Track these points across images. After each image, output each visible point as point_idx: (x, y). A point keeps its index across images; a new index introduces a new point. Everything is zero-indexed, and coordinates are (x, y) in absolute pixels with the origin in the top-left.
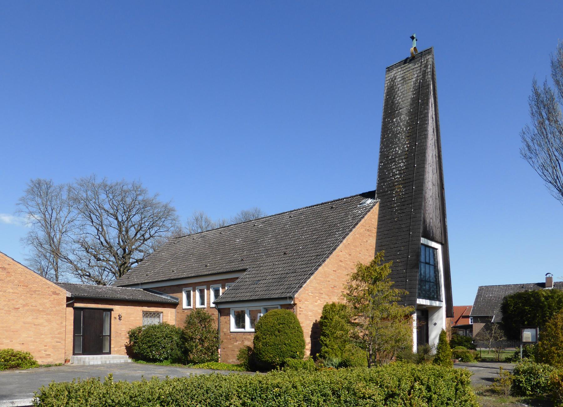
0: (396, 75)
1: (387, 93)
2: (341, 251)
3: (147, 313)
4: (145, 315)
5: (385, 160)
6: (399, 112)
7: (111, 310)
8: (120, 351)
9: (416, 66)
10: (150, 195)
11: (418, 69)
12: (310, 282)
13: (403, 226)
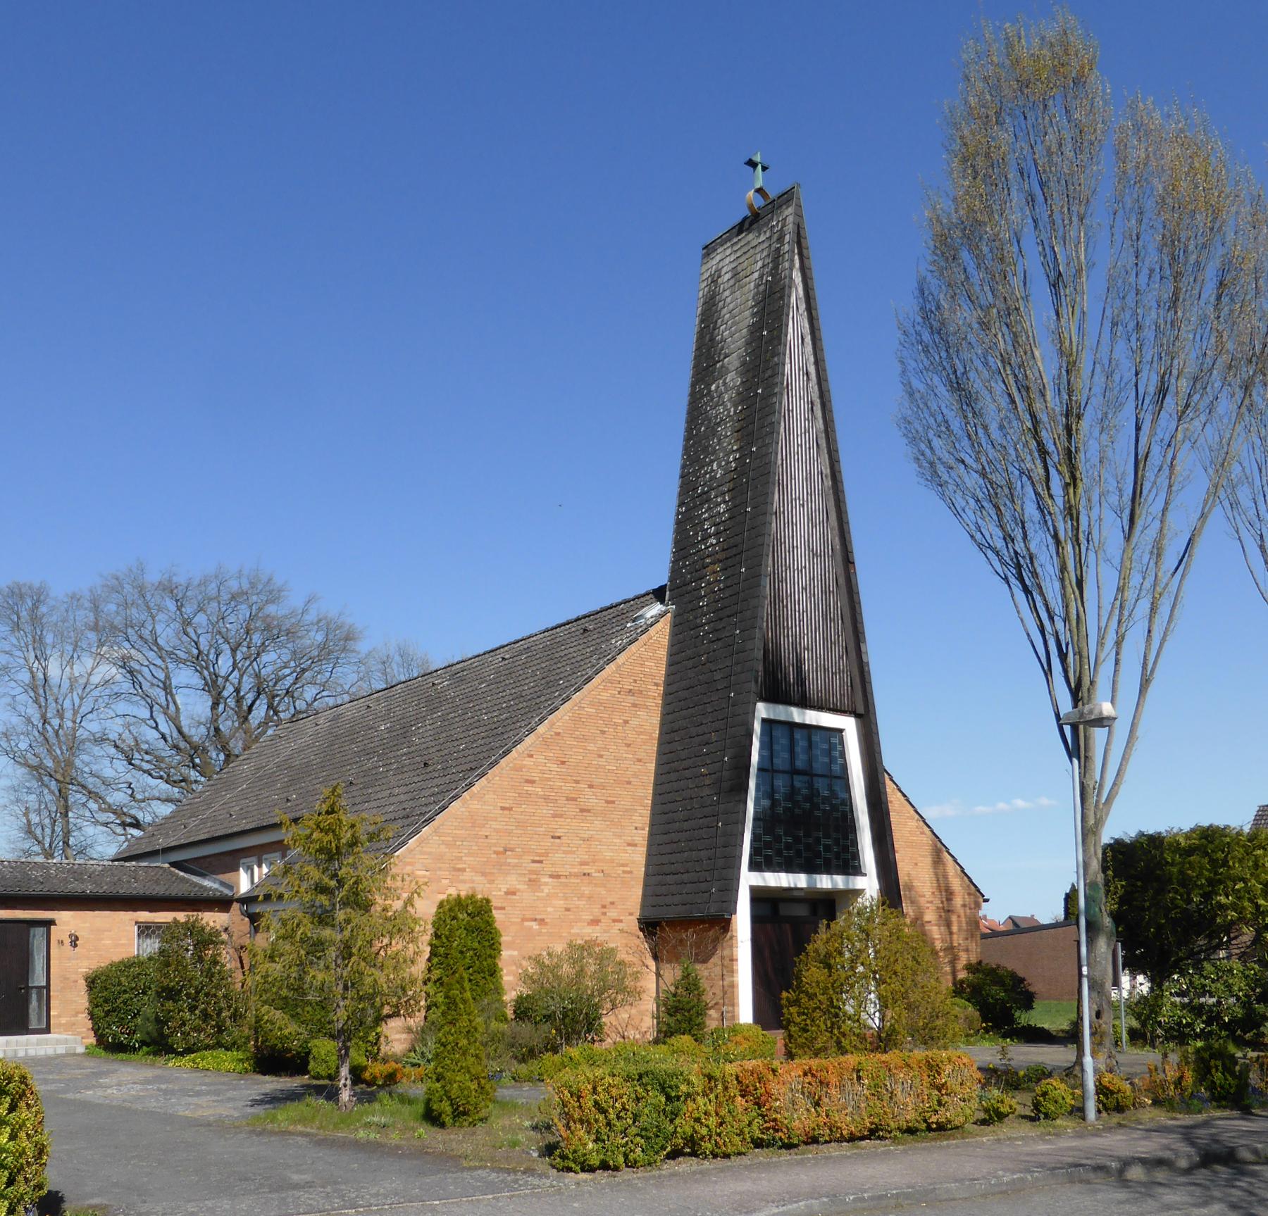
0: (721, 264)
1: (702, 314)
2: (531, 756)
3: (148, 928)
4: (143, 932)
5: (689, 496)
6: (722, 366)
7: (50, 923)
8: (74, 1024)
9: (762, 238)
10: (293, 600)
11: (766, 245)
12: (420, 842)
13: (717, 676)
